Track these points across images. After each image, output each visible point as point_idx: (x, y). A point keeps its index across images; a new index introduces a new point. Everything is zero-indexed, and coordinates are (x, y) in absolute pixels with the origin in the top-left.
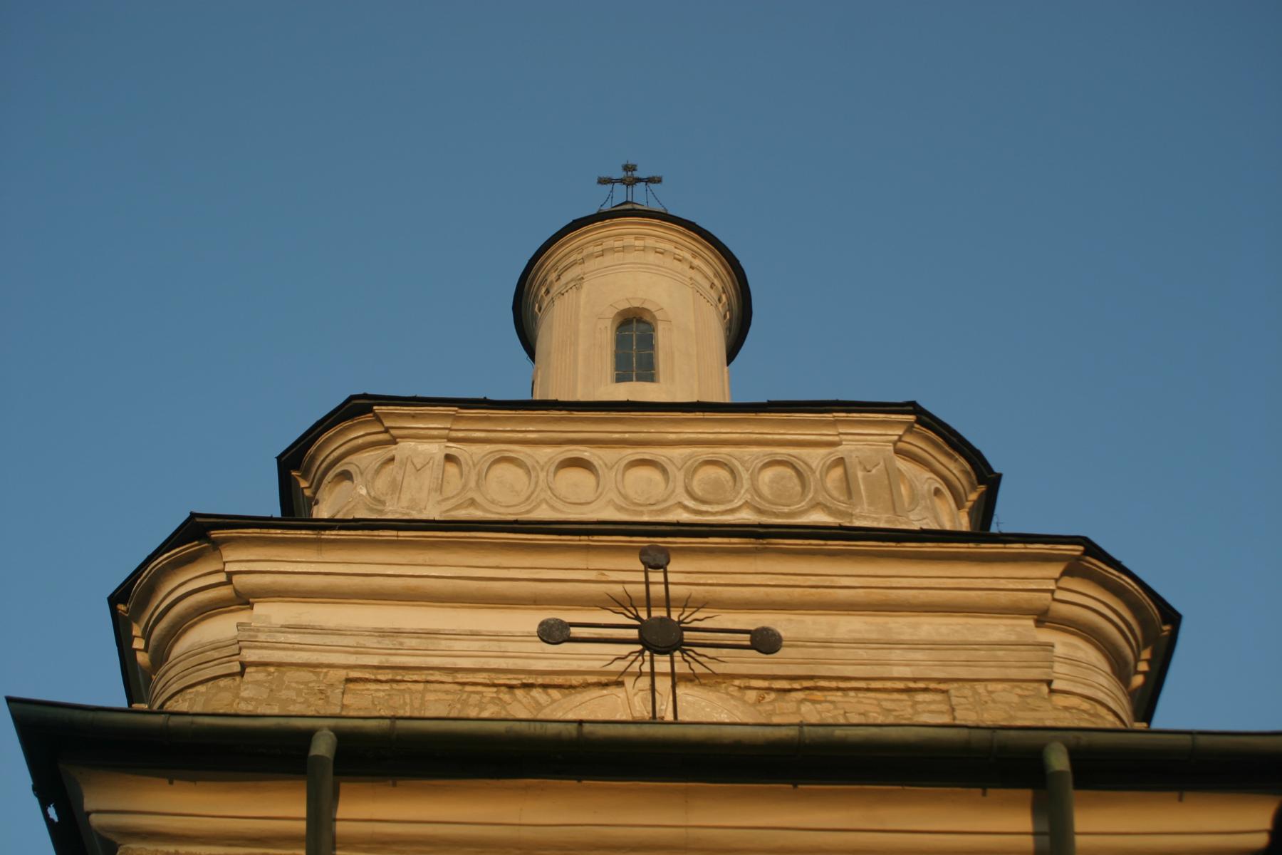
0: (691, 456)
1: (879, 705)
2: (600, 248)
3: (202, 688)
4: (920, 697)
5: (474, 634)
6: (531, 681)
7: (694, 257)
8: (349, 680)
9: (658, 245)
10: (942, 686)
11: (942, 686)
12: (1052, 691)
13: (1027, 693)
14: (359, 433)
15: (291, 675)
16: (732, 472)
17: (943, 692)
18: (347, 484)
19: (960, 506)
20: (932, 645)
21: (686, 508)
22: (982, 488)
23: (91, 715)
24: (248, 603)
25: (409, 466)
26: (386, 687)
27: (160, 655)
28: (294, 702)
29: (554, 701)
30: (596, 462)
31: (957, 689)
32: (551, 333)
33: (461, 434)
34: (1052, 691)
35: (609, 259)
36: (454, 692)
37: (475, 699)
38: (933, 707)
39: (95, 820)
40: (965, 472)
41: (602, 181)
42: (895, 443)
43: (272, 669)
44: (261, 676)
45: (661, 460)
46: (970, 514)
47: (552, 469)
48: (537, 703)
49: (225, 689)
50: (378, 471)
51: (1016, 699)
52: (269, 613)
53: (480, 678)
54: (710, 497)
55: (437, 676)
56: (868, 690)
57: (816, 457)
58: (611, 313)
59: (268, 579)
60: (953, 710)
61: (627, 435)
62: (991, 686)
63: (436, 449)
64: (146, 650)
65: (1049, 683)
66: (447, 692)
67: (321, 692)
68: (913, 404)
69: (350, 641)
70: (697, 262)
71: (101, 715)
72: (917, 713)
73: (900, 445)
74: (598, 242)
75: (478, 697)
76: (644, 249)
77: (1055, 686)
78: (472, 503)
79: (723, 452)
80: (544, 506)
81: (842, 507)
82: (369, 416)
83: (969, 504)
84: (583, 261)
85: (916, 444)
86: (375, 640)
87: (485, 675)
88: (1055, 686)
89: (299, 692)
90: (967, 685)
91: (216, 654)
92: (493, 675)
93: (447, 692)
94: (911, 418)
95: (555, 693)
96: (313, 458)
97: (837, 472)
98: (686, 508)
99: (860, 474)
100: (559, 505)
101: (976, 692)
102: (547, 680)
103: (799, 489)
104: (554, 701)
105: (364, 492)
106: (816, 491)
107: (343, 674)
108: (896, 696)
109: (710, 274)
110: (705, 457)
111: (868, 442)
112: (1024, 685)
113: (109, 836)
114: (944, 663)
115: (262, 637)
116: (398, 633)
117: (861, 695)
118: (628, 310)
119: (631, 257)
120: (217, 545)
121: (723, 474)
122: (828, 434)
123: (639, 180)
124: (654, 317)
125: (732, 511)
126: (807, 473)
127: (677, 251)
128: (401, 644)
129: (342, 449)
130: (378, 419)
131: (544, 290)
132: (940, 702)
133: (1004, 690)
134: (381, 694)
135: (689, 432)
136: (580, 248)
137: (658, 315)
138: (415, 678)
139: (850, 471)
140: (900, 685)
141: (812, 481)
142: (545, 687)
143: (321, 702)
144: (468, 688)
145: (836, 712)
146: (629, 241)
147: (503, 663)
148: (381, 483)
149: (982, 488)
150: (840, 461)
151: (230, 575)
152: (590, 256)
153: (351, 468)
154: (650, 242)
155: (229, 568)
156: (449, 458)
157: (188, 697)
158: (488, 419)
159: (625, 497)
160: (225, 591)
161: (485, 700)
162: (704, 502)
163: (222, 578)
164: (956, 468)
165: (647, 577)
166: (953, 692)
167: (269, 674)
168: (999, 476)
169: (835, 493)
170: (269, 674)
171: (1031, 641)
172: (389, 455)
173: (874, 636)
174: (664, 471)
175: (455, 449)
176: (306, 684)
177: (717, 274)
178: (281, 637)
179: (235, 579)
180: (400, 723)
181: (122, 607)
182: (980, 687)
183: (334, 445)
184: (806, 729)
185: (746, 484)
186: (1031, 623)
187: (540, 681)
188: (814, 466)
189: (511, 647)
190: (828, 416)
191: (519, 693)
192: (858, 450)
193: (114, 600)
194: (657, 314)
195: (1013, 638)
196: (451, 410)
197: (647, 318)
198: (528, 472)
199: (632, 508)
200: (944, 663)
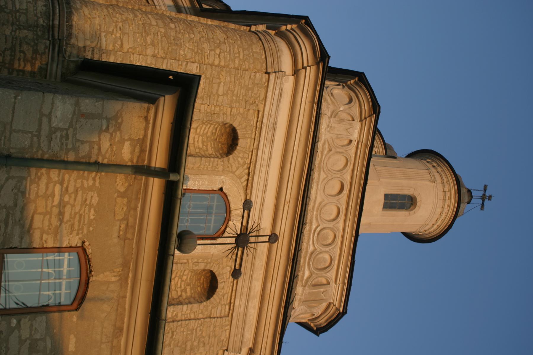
0: (338, 230)
1: (226, 293)
2: (447, 190)
3: (263, 57)
4: (227, 307)
5: (270, 157)
6: (250, 175)
7: (438, 226)
8: (259, 111)
9: (444, 213)
10: (230, 315)
11: (230, 315)
12: (224, 350)
13: (224, 342)
14: (366, 107)
15: (263, 91)
16: (330, 244)
17: (228, 315)
18: (347, 101)
19: (309, 320)
21: (317, 227)
22: (315, 329)
23: (192, 104)
24: (295, 74)
25: (349, 127)
26: (255, 125)
27: (282, 35)
28: (252, 93)
29: (242, 183)
30: (341, 196)
31: (228, 320)
32: (417, 167)
33: (360, 146)
34: (224, 350)
35: (441, 194)
36: (249, 149)
37: (246, 156)
38: (223, 311)
39: (162, 99)
40: (321, 324)
41: (485, 187)
42: (333, 303)
43: (266, 84)
44: (264, 80)
45: (339, 219)
46: (306, 322)
47: (340, 180)
48: (242, 177)
49: (262, 66)
50: (349, 114)
51: (222, 338)
52: (289, 83)
53: (254, 158)
54: (320, 236)
55: (256, 143)
56: (232, 290)
57: (332, 274)
58: (416, 194)
59: (302, 82)
60: (221, 318)
61: (350, 207)
62: (228, 331)
63: (355, 136)
64: (287, 30)
65: (227, 350)
66: (250, 146)
67: (255, 102)
68: (346, 312)
69: (273, 113)
70: (435, 227)
71: (192, 107)
72: (222, 305)
73: (332, 305)
74: (449, 190)
75: (247, 157)
76: (443, 208)
77: (226, 351)
78: (330, 150)
80: (325, 176)
81: (309, 283)
82: (372, 112)
83: (310, 323)
84: (443, 183)
85: (332, 310)
86: (273, 121)
87: (255, 160)
88: (226, 351)
89: (256, 94)
90: (229, 323)
91: (276, 62)
92: (254, 162)
93: (250, 146)
94: (341, 311)
95: (245, 183)
96: (361, 87)
97: (325, 282)
98: (317, 227)
99: (322, 290)
100: (325, 182)
101: (226, 326)
102: (250, 181)
103: (320, 267)
104: (242, 183)
105: (341, 109)
106: (317, 274)
108: (229, 299)
109: (430, 230)
110: (337, 235)
111: (334, 294)
112: (227, 342)
113: (157, 103)
114: (238, 317)
115: (279, 81)
116: (274, 129)
117: (231, 287)
118: (416, 200)
119: (440, 203)
120: (318, 64)
121: (330, 241)
123: (483, 201)
124: (412, 210)
125: (313, 244)
127: (441, 220)
128: (270, 131)
129: (361, 100)
130: (370, 116)
131: (435, 165)
132: (225, 313)
133: (226, 335)
134: (252, 123)
135: (348, 230)
136: (448, 182)
137: (412, 212)
138: (257, 135)
139: (324, 286)
140: (232, 301)
141: (322, 273)
142: (248, 180)
143: (251, 102)
144: (250, 153)
145: (225, 279)
146: (448, 202)
147: (258, 166)
148: (344, 116)
149: (315, 329)
150: (328, 283)
151: (305, 68)
152: (444, 186)
153: (353, 104)
154: (446, 210)
155: (308, 68)
156: (351, 141)
157: (261, 51)
158: (364, 157)
159: (325, 206)
160: (300, 66)
161: (245, 159)
162: (318, 234)
163: (305, 65)
164: (322, 321)
165: (171, 322)
166: (227, 318)
167: (265, 83)
168: (318, 336)
169: (316, 280)
170: (265, 83)
171: (243, 346)
173: (252, 294)
174: (334, 220)
175: (354, 144)
176: (259, 97)
177: (430, 233)
178: (278, 88)
179: (304, 70)
180: (179, 201)
181: (303, 21)
182: (228, 327)
183: (364, 97)
184: (164, 322)
185: (323, 249)
186: (250, 346)
187: (250, 179)
188: (328, 274)
189: (264, 170)
190: (346, 281)
191: (247, 171)
192: (332, 290)
193: (306, 18)
194: (413, 211)
195: (245, 340)
196: (369, 144)
197: (412, 207)
198: (340, 170)
199: (320, 208)
200: (238, 317)
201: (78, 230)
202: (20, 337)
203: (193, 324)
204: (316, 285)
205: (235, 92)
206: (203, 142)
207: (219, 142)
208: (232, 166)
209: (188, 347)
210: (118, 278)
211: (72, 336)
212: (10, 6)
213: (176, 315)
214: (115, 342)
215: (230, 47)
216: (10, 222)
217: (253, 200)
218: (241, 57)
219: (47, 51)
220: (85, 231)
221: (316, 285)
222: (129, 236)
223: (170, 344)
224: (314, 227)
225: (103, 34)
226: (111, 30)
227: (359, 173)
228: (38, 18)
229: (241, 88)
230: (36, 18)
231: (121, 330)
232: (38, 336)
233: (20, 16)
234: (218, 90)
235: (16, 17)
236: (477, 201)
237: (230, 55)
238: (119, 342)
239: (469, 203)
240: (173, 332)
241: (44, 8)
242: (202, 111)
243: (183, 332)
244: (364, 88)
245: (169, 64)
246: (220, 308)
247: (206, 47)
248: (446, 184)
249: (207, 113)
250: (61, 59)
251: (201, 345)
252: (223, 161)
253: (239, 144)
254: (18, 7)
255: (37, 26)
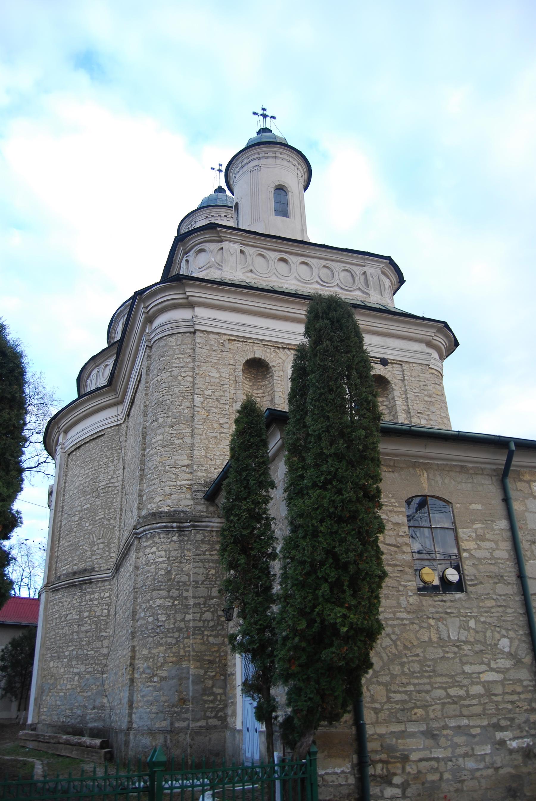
3: (180, 335)
4: (394, 365)
5: (268, 329)
8: (229, 340)
14: (208, 236)
16: (332, 271)
20: (401, 350)
35: (271, 161)
41: (255, 113)
44: (202, 335)
52: (200, 311)
54: (325, 280)
57: (358, 271)
58: (273, 186)
63: (237, 247)
70: (300, 167)
78: (251, 271)
79: (329, 263)
82: (214, 231)
91: (184, 324)
94: (388, 261)
100: (279, 276)
103: (351, 281)
107: (228, 337)
114: (402, 356)
115: (201, 321)
119: (279, 161)
120: (184, 286)
122: (361, 262)
125: (333, 286)
126: (355, 276)
151: (188, 296)
154: (285, 156)
155: (188, 293)
172: (221, 247)
176: (217, 339)
177: (303, 171)
179: (190, 298)
182: (411, 365)
191: (281, 350)
200: (402, 356)
201: (393, 506)
202: (475, 549)
203: (410, 395)
204: (367, 283)
205: (216, 361)
206: (258, 389)
207: (256, 375)
208: (278, 363)
209: (429, 399)
210: (425, 472)
211: (471, 507)
212: (164, 566)
213: (404, 410)
214: (471, 471)
215: (174, 367)
216: (394, 562)
217: (298, 343)
218: (183, 356)
219: (201, 532)
220: (393, 500)
221: (367, 283)
222: (392, 464)
223: (428, 415)
224: (318, 287)
225: (179, 483)
226: (174, 476)
227: (270, 244)
228: (172, 541)
229: (211, 356)
230: (172, 543)
231: (462, 467)
232: (474, 535)
233: (172, 557)
234: (216, 378)
235: (174, 560)
236: (269, 124)
237: (182, 367)
238: (471, 468)
239: (270, 131)
240: (418, 413)
241: (162, 536)
242: (234, 391)
243: (417, 404)
244: (191, 237)
245: (199, 423)
246: (396, 372)
247: (177, 389)
248: (261, 156)
249: (236, 387)
250: (204, 519)
251: (426, 388)
252: (275, 371)
253: (260, 357)
254: (164, 559)
255: (180, 541)
